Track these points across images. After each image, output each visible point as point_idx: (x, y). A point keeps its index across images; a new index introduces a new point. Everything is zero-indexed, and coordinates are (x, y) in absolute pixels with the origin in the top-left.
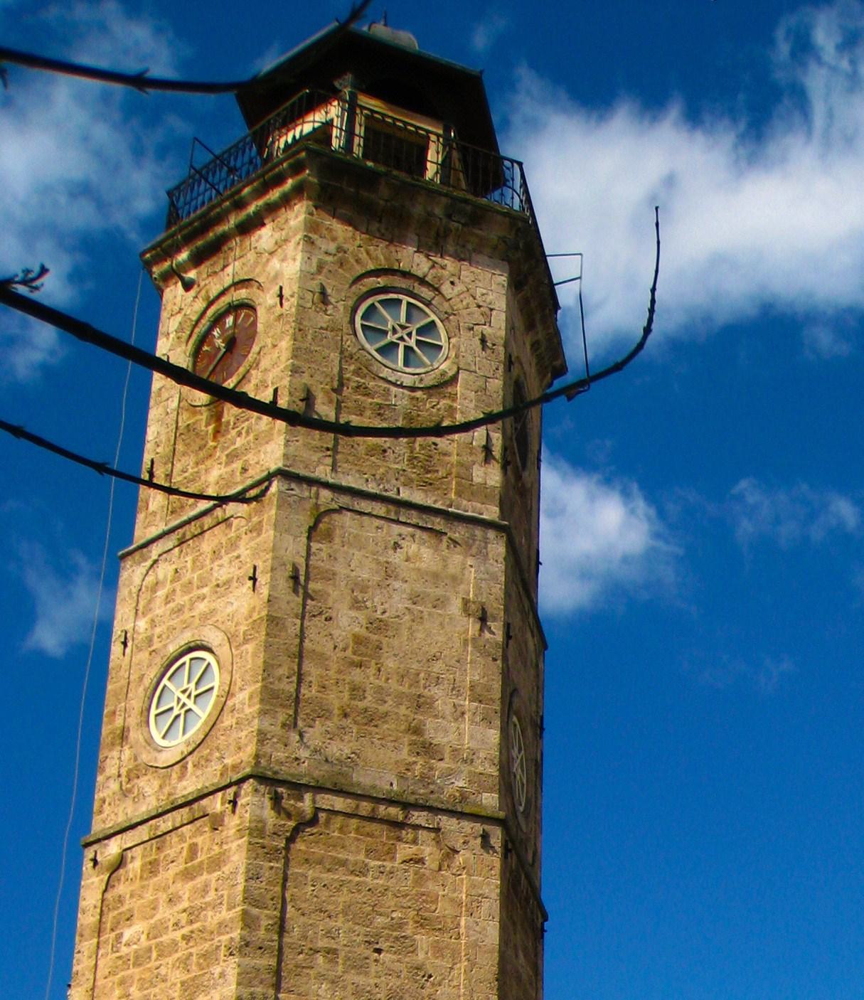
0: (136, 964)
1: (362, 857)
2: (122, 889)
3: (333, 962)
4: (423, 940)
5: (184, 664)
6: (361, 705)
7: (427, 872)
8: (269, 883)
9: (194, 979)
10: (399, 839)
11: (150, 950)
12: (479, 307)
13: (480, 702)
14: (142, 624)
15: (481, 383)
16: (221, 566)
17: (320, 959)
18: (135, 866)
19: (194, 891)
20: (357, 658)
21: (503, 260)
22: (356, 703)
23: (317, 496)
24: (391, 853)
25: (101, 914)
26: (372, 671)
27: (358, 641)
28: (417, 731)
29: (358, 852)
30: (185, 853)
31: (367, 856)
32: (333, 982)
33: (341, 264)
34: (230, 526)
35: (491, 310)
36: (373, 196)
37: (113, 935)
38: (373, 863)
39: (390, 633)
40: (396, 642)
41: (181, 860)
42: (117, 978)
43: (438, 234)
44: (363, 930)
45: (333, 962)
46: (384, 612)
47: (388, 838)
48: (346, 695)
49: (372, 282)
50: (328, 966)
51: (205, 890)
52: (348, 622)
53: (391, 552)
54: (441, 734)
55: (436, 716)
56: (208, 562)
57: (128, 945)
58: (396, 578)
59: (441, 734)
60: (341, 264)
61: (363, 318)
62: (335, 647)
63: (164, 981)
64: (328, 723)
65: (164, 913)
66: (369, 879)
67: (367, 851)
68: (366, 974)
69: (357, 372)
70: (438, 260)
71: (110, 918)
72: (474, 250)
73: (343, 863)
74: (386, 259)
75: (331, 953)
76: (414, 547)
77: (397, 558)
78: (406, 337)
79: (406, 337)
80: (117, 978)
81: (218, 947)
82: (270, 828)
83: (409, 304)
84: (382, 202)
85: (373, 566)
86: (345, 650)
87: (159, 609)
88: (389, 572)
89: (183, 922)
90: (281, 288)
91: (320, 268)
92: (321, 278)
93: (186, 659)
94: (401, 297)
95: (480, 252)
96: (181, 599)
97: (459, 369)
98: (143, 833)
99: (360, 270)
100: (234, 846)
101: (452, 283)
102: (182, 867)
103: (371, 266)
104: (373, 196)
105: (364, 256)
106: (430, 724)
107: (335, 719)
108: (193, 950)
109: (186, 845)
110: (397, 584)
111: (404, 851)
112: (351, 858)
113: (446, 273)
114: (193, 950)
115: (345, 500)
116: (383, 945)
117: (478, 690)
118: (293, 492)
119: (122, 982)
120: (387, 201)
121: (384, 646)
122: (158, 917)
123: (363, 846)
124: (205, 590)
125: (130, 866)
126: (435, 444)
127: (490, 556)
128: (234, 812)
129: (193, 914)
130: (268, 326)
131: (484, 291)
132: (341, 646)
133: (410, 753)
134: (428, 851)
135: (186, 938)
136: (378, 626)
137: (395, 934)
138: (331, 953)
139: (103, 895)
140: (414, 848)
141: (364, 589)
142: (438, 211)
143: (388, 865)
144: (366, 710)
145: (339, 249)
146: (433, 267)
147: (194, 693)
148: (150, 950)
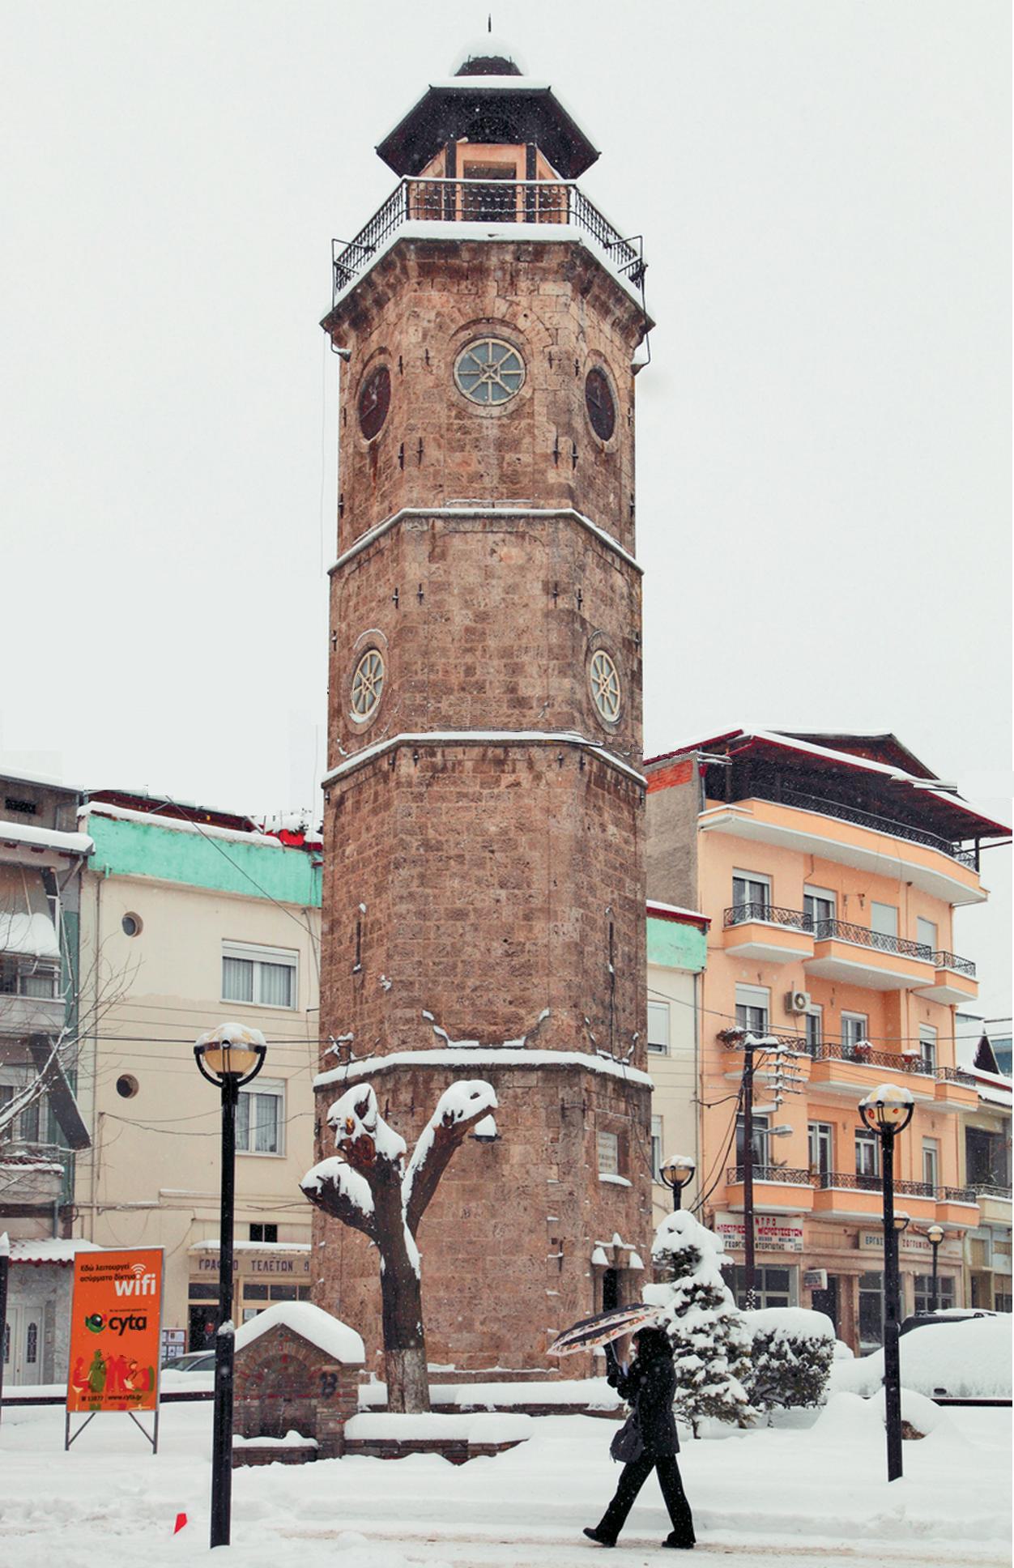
0: (353, 872)
1: (478, 788)
2: (343, 819)
3: (462, 863)
4: (523, 839)
5: (366, 659)
6: (473, 679)
7: (523, 792)
8: (417, 817)
9: (381, 882)
10: (503, 771)
11: (358, 862)
12: (547, 329)
13: (557, 659)
14: (344, 626)
15: (551, 398)
16: (380, 586)
17: (452, 862)
18: (349, 804)
19: (378, 823)
20: (468, 646)
21: (564, 280)
22: (469, 678)
23: (433, 527)
24: (497, 781)
25: (334, 836)
26: (479, 653)
27: (468, 630)
28: (513, 690)
29: (475, 786)
30: (372, 797)
31: (481, 787)
32: (463, 877)
33: (441, 327)
34: (383, 555)
35: (557, 329)
36: (457, 262)
37: (340, 851)
38: (486, 792)
39: (491, 621)
40: (496, 627)
41: (371, 802)
42: (343, 880)
43: (512, 275)
44: (480, 839)
45: (462, 863)
46: (486, 605)
47: (495, 772)
48: (462, 674)
49: (464, 335)
50: (459, 867)
51: (382, 823)
52: (461, 618)
53: (489, 557)
54: (530, 689)
55: (526, 677)
56: (373, 582)
57: (348, 858)
58: (493, 577)
59: (530, 689)
60: (441, 327)
61: (459, 370)
62: (453, 640)
63: (367, 883)
64: (451, 697)
65: (365, 836)
66: (483, 803)
67: (481, 783)
68: (484, 868)
69: (457, 417)
70: (514, 298)
71: (338, 839)
72: (541, 280)
73: (465, 795)
74: (473, 312)
75: (460, 858)
76: (505, 549)
77: (492, 561)
78: (492, 375)
79: (492, 375)
80: (343, 880)
81: (390, 863)
82: (415, 780)
83: (493, 344)
84: (465, 264)
85: (476, 571)
86: (460, 640)
87: (352, 616)
88: (488, 573)
89: (374, 844)
90: (401, 357)
91: (425, 336)
92: (426, 345)
93: (368, 655)
94: (487, 340)
95: (546, 280)
96: (363, 610)
97: (534, 390)
98: (351, 782)
99: (454, 327)
100: (395, 793)
101: (525, 316)
102: (371, 806)
103: (463, 322)
104: (457, 262)
105: (457, 315)
106: (522, 682)
107: (456, 693)
108: (379, 864)
109: (372, 791)
110: (494, 582)
111: (508, 779)
112: (471, 790)
113: (520, 308)
114: (379, 864)
115: (453, 525)
116: (495, 847)
117: (556, 650)
118: (351, 609)
119: (347, 883)
120: (468, 262)
121: (487, 631)
122: (362, 840)
123: (478, 781)
124: (374, 604)
125: (346, 804)
126: (519, 459)
127: (561, 542)
128: (393, 770)
129: (378, 838)
130: (397, 390)
131: (551, 314)
132: (457, 638)
133: (508, 707)
134: (524, 776)
135: (376, 855)
136: (482, 617)
137: (503, 838)
138: (460, 858)
139: (335, 823)
140: (514, 776)
141: (471, 591)
142: (509, 258)
143: (496, 791)
144: (477, 683)
145: (438, 314)
146: (511, 305)
147: (374, 681)
148: (358, 862)
